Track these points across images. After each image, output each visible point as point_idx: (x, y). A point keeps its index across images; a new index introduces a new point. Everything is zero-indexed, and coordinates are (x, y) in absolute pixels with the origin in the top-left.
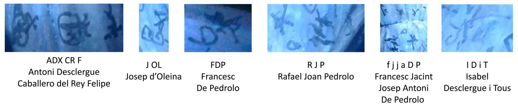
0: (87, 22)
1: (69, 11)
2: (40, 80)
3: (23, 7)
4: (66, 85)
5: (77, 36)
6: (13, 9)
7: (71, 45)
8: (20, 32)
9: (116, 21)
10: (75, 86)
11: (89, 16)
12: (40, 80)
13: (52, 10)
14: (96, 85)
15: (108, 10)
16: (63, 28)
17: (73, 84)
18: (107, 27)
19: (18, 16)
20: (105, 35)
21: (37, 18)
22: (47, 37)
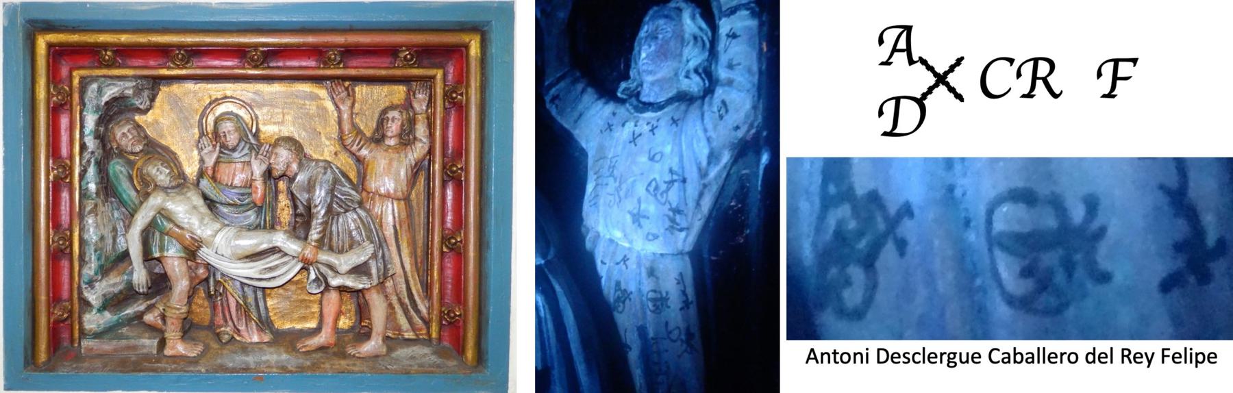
0: (1095, 225)
1: (1028, 185)
2: (1044, 348)
3: (855, 169)
4: (1108, 360)
5: (1060, 278)
6: (818, 179)
7: (1037, 312)
8: (845, 266)
9: (1202, 224)
10: (1131, 362)
11: (1104, 203)
12: (1044, 348)
13: (963, 183)
14: (1182, 360)
15: (1173, 181)
16: (1005, 248)
17: (1126, 359)
18: (1170, 247)
19: (836, 206)
20: (1164, 275)
21: (907, 210)
22: (946, 282)
